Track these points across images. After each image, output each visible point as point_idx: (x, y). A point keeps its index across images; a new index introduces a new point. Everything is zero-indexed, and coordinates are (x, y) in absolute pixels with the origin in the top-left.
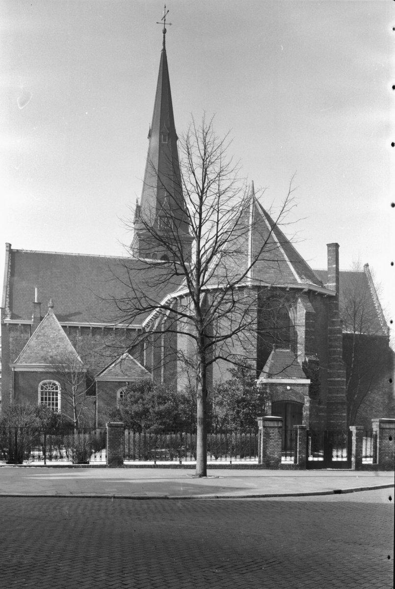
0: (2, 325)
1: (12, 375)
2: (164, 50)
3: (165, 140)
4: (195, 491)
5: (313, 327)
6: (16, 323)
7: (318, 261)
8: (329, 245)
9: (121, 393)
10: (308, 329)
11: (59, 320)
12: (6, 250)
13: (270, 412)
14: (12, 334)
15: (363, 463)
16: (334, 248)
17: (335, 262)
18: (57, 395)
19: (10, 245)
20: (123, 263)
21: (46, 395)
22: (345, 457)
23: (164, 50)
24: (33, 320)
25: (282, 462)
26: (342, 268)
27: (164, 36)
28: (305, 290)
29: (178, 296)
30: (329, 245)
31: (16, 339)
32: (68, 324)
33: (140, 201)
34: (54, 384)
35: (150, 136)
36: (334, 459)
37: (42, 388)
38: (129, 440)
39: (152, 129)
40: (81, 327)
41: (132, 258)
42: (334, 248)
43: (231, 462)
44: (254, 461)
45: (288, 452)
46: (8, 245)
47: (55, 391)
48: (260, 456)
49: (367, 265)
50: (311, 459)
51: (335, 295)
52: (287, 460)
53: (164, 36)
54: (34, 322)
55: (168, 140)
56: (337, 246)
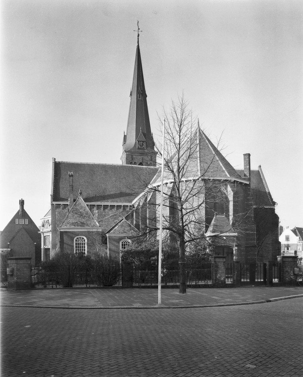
0: (51, 205)
1: (59, 233)
2: (138, 46)
3: (140, 97)
4: (253, 302)
5: (238, 202)
6: (59, 203)
7: (238, 164)
8: (245, 155)
9: (122, 243)
10: (234, 203)
11: (85, 201)
12: (53, 162)
13: (45, 248)
14: (57, 210)
15: (273, 282)
16: (248, 156)
17: (248, 165)
18: (85, 245)
19: (55, 159)
20: (122, 167)
21: (78, 245)
22: (225, 279)
23: (138, 46)
24: (69, 202)
25: (226, 283)
26: (252, 169)
27: (138, 38)
28: (232, 181)
29: (156, 186)
30: (245, 155)
31: (60, 213)
32: (89, 204)
33: (125, 133)
34: (83, 238)
35: (131, 95)
36: (256, 280)
37: (76, 241)
38: (261, 273)
39: (132, 91)
40: (103, 205)
41: (125, 164)
42: (248, 156)
43: (196, 283)
44: (210, 283)
45: (230, 276)
46: (54, 159)
47: (83, 242)
48: (213, 279)
49: (260, 166)
50: (242, 280)
51: (248, 183)
52: (229, 281)
53: (138, 38)
54: (70, 202)
55: (142, 97)
56: (249, 155)
